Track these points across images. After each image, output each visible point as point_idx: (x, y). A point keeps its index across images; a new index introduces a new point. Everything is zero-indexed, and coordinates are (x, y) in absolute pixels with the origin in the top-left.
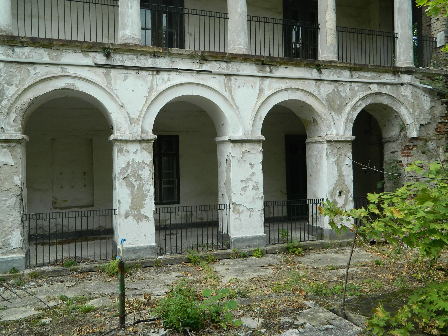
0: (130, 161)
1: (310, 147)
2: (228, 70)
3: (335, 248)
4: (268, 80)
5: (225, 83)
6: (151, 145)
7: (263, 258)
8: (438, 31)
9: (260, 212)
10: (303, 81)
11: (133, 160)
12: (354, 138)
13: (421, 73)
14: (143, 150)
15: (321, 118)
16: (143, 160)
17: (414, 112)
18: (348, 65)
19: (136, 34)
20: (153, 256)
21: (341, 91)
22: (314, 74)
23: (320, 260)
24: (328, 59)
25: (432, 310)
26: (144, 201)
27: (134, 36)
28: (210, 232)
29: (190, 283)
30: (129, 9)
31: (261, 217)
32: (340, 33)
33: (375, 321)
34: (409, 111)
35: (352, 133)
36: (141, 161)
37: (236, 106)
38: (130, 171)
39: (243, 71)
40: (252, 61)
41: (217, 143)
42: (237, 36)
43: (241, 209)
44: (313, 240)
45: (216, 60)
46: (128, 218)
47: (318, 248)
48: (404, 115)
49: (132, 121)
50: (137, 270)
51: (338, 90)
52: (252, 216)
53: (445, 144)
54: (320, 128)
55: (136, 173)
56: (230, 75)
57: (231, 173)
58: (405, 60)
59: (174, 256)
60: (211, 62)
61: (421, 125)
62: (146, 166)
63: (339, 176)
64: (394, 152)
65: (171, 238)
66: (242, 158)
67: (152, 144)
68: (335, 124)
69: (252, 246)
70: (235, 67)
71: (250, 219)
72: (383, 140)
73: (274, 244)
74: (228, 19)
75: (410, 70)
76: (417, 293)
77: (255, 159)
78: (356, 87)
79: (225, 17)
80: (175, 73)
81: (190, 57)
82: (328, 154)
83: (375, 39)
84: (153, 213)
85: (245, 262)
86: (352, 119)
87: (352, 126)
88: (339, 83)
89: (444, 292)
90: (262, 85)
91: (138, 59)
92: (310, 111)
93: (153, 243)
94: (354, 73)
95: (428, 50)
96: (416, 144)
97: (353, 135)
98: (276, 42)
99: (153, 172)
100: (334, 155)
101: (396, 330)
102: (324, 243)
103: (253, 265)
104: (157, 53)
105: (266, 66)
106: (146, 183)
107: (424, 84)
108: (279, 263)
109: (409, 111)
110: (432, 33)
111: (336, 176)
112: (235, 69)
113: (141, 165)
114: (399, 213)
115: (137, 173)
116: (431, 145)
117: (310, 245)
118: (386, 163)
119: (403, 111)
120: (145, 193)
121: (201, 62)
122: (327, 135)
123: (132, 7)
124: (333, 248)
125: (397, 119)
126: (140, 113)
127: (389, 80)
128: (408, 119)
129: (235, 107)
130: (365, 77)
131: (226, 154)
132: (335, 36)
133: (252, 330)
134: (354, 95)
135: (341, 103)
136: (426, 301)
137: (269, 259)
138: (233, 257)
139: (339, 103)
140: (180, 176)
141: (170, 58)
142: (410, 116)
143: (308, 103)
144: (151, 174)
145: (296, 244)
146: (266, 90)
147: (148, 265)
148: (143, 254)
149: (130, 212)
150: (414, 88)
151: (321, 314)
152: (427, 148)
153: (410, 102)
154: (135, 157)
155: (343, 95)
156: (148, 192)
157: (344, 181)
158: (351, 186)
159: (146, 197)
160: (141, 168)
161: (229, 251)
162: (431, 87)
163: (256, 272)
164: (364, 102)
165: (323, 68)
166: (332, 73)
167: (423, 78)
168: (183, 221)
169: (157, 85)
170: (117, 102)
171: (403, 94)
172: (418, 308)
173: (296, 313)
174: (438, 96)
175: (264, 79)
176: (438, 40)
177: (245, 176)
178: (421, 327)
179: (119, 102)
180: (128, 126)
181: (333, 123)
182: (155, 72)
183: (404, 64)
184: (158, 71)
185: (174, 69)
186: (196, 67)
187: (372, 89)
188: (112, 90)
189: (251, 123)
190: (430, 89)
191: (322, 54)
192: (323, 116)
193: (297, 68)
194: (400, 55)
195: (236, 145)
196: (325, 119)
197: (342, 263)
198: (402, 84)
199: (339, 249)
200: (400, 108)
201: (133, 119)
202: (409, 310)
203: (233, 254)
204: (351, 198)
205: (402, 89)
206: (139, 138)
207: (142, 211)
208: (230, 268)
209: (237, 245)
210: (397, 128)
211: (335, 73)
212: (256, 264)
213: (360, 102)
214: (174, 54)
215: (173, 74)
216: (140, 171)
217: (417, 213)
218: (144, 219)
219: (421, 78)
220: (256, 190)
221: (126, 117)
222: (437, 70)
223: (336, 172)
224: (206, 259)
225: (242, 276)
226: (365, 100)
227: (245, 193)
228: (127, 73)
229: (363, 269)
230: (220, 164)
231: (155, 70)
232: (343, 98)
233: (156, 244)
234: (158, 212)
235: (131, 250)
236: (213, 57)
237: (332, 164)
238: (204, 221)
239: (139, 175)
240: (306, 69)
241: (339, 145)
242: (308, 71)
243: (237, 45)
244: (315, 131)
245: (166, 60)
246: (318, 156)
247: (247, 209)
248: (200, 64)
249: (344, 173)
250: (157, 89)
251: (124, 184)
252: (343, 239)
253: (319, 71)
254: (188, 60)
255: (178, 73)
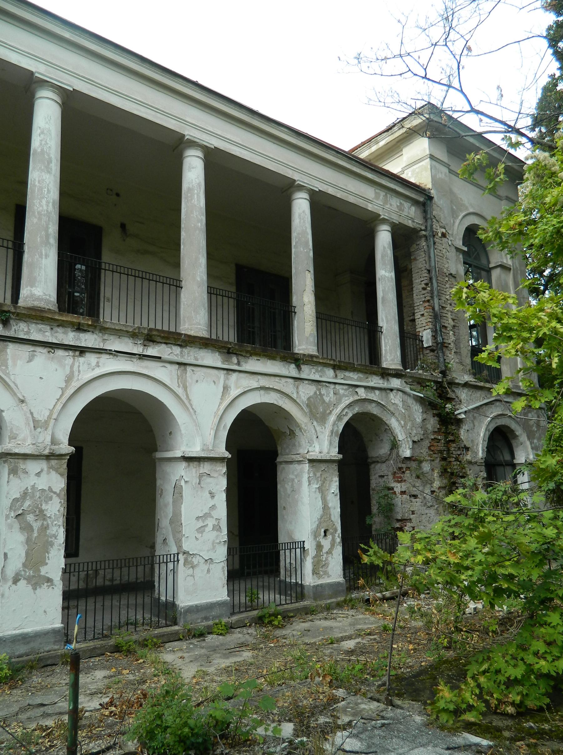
0: (29, 488)
1: (284, 468)
2: (182, 357)
3: (321, 612)
4: (234, 376)
5: (178, 375)
6: (64, 462)
7: (228, 635)
8: (424, 328)
9: (222, 564)
10: (279, 378)
11: (33, 487)
12: (341, 456)
13: (411, 377)
14: (51, 470)
15: (300, 429)
16: (50, 487)
17: (406, 424)
18: (332, 362)
19: (50, 295)
20: (58, 645)
21: (324, 394)
22: (291, 370)
23: (309, 631)
24: (306, 352)
25: (500, 681)
26: (48, 553)
27: (48, 297)
28: (124, 602)
29: (132, 684)
30: (42, 258)
31: (224, 571)
32: (319, 320)
33: (441, 704)
34: (400, 423)
35: (337, 450)
36: (47, 488)
37: (193, 409)
38: (27, 503)
39: (203, 359)
40: (215, 348)
41: (157, 460)
42: (194, 312)
43: (195, 561)
44: (291, 603)
45: (167, 342)
46: (18, 584)
47: (300, 614)
48: (395, 428)
49: (36, 424)
50: (31, 673)
51: (320, 393)
52: (211, 572)
53: (439, 466)
54: (299, 442)
55: (37, 507)
56: (185, 364)
57: (183, 506)
58: (392, 360)
59: (91, 644)
60: (160, 344)
61: (414, 442)
62: (54, 496)
63: (324, 508)
64: (383, 476)
65: (68, 615)
66: (199, 484)
67: (67, 460)
68: (317, 437)
69: (211, 618)
70: (191, 353)
71: (208, 575)
72: (369, 460)
73: (240, 612)
74: (182, 288)
75: (400, 372)
76: (477, 661)
77: (217, 484)
78: (341, 390)
79: (178, 285)
80: (107, 356)
81: (130, 335)
82: (310, 479)
83: (346, 329)
84: (61, 573)
85: (204, 644)
86: (337, 431)
87: (337, 441)
88: (321, 384)
89: (511, 655)
90: (227, 381)
91: (53, 332)
92: (286, 418)
93: (58, 624)
94: (338, 372)
95: (412, 349)
96: (409, 466)
97: (339, 453)
98: (226, 322)
99: (65, 505)
100: (317, 479)
101: (467, 713)
102: (308, 606)
103: (217, 647)
104: (83, 326)
105: (232, 355)
106: (52, 523)
107: (415, 391)
108: (254, 641)
109: (400, 423)
110: (417, 330)
111: (320, 509)
112: (192, 357)
113: (47, 494)
114: (455, 555)
115: (39, 508)
116: (426, 467)
117: (290, 611)
118: (374, 490)
119: (394, 423)
120: (50, 539)
121: (146, 343)
122: (308, 452)
123: (47, 256)
124: (319, 613)
125: (387, 433)
126: (50, 413)
127: (377, 383)
128: (401, 436)
129: (191, 410)
130: (351, 379)
131: (174, 478)
132: (315, 324)
133: (287, 740)
134: (339, 401)
135: (325, 411)
136: (491, 670)
137: (237, 636)
138: (183, 637)
139: (321, 410)
140: (81, 511)
141: (101, 334)
142: (402, 430)
143: (286, 409)
144: (62, 509)
145: (272, 610)
146: (232, 388)
147: (49, 662)
148: (41, 644)
149: (23, 573)
150: (404, 395)
151: (363, 706)
152: (421, 471)
153: (401, 412)
154: (37, 482)
155: (327, 399)
156: (56, 538)
157: (330, 515)
158: (338, 523)
159: (52, 546)
160: (46, 500)
161: (176, 628)
162: (422, 396)
163: (228, 658)
164: (351, 411)
165: (303, 364)
166: (313, 371)
167: (413, 384)
168: (82, 585)
169: (79, 371)
170: (14, 394)
171: (393, 401)
172: (486, 680)
173: (331, 708)
174: (429, 407)
175: (230, 372)
176: (424, 339)
177: (202, 511)
178: (493, 705)
179: (18, 395)
180: (31, 432)
181: (315, 437)
182: (77, 353)
183: (391, 364)
184: (82, 351)
185: (106, 350)
186: (138, 349)
187: (359, 393)
188: (8, 375)
189: (213, 433)
190: (421, 397)
191: (299, 345)
192: (303, 426)
193: (271, 361)
194: (385, 354)
195: (191, 464)
196: (305, 431)
197: (340, 633)
198: (392, 390)
199: (328, 614)
200: (390, 420)
201: (38, 421)
202: (476, 684)
203: (183, 632)
204: (338, 540)
205: (392, 395)
206: (46, 452)
207: (44, 571)
208: (185, 655)
209: (189, 617)
210: (387, 445)
211: (317, 371)
212: (222, 645)
213: (346, 410)
214: (108, 328)
215: (104, 357)
216: (44, 505)
217: (474, 555)
218: (46, 584)
219: (411, 383)
220: (217, 530)
221: (27, 419)
222: (427, 375)
223: (320, 504)
224: (144, 644)
225: (210, 666)
226: (351, 408)
227: (202, 536)
228: (34, 351)
229: (371, 639)
230: (162, 492)
231: (78, 350)
232: (326, 403)
233: (62, 625)
234: (68, 571)
235: (20, 638)
236: (163, 338)
237: (315, 491)
238: (115, 583)
239: (41, 511)
240: (282, 363)
241: (323, 466)
242: (284, 367)
243: (195, 324)
244: (290, 447)
245: (95, 336)
246: (296, 481)
247: (204, 561)
248: (145, 346)
249: (330, 505)
250: (80, 378)
251: (17, 525)
252: (331, 598)
253: (298, 367)
254: (126, 340)
255: (111, 356)
